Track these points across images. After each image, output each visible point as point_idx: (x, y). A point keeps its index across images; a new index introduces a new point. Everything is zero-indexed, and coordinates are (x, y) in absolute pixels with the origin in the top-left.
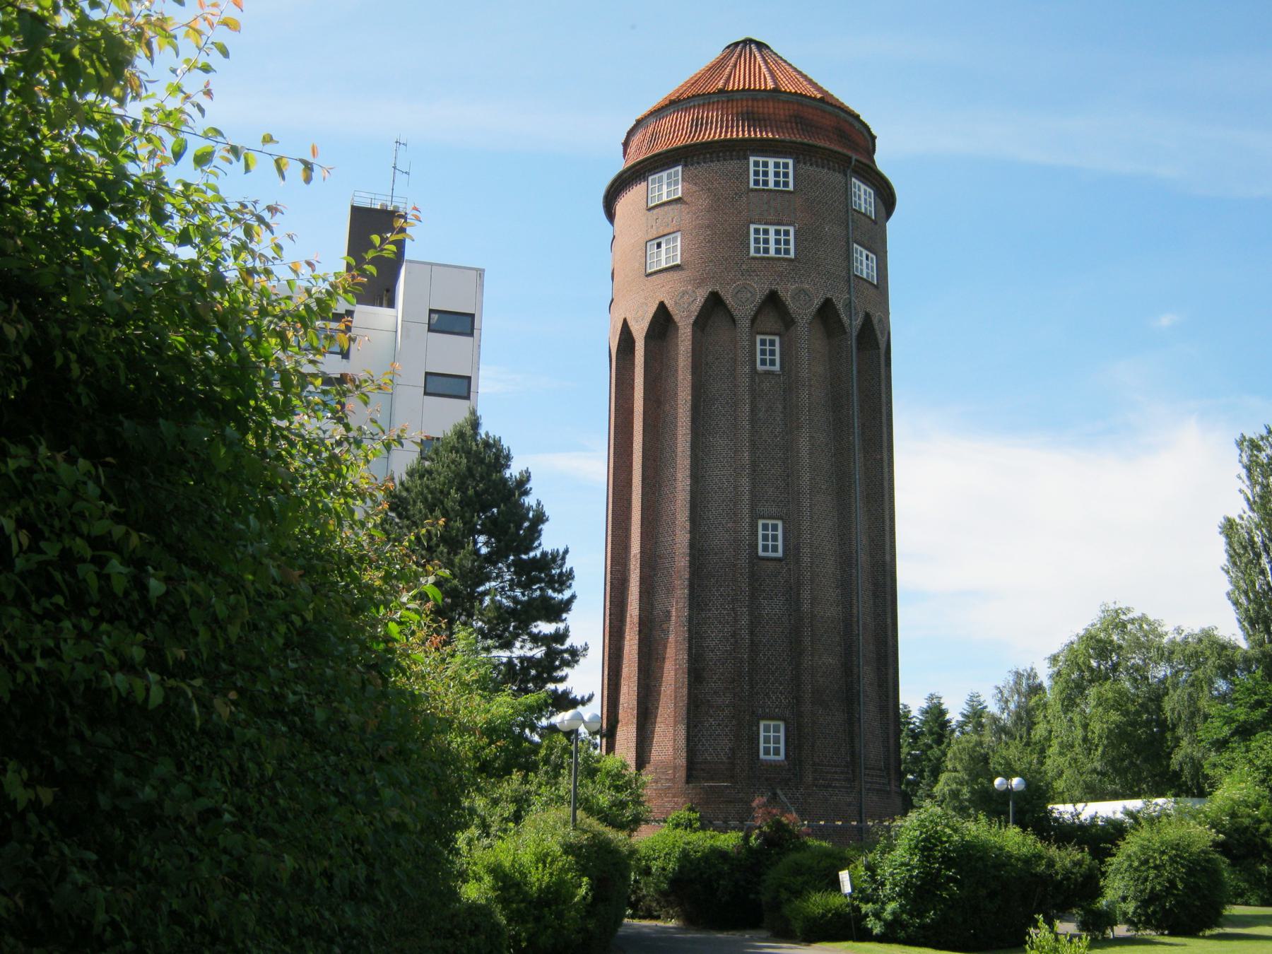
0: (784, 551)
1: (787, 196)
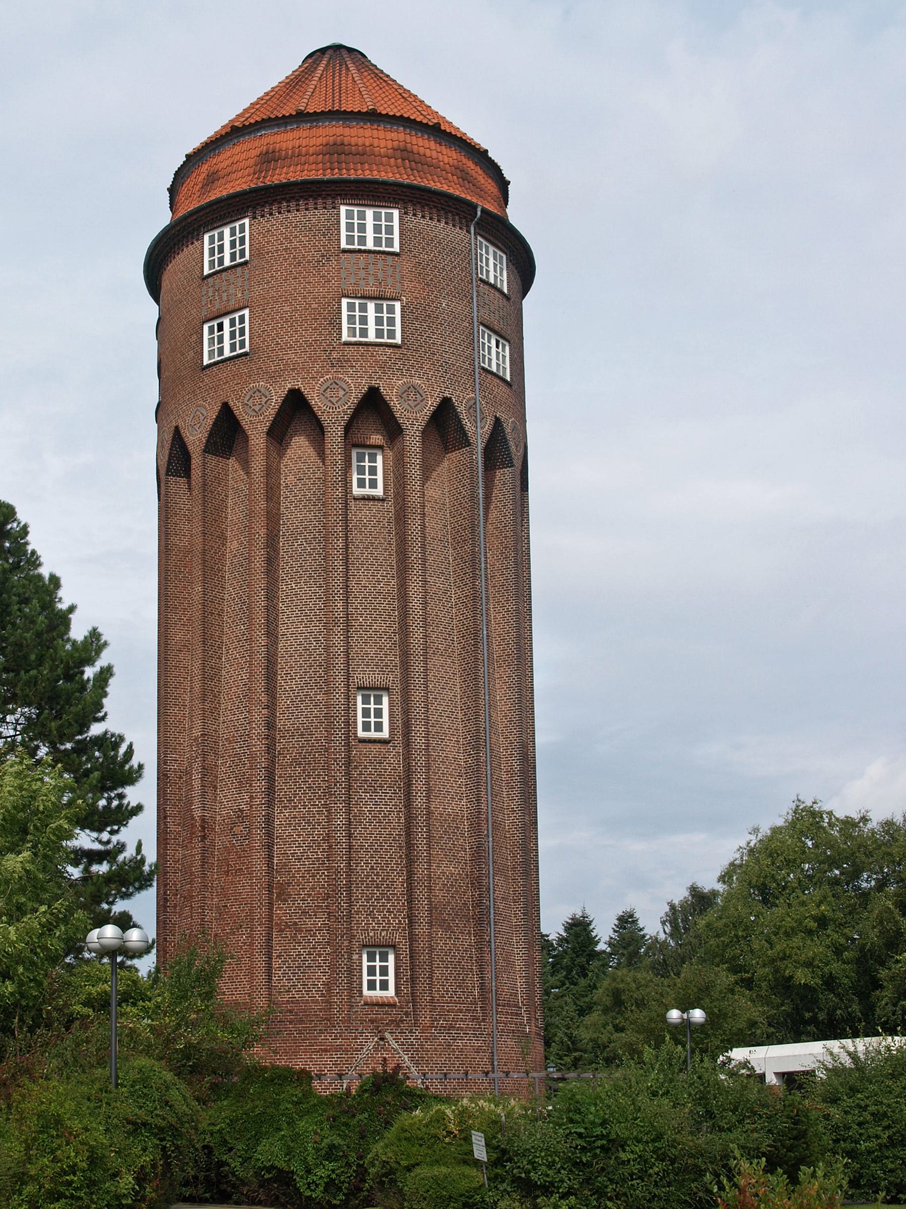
1: (390, 258)
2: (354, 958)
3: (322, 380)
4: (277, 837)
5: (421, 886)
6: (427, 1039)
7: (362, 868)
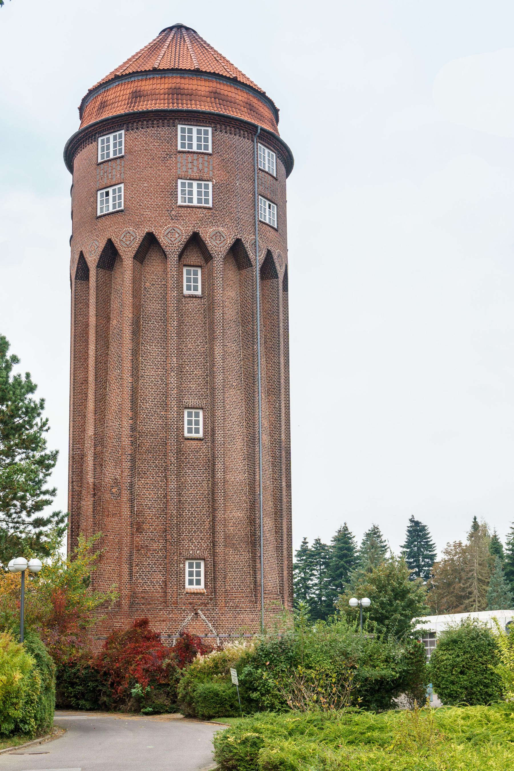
0: (205, 432)
1: (206, 157)
2: (181, 566)
3: (166, 227)
4: (137, 495)
5: (220, 524)
6: (222, 614)
7: (186, 514)
